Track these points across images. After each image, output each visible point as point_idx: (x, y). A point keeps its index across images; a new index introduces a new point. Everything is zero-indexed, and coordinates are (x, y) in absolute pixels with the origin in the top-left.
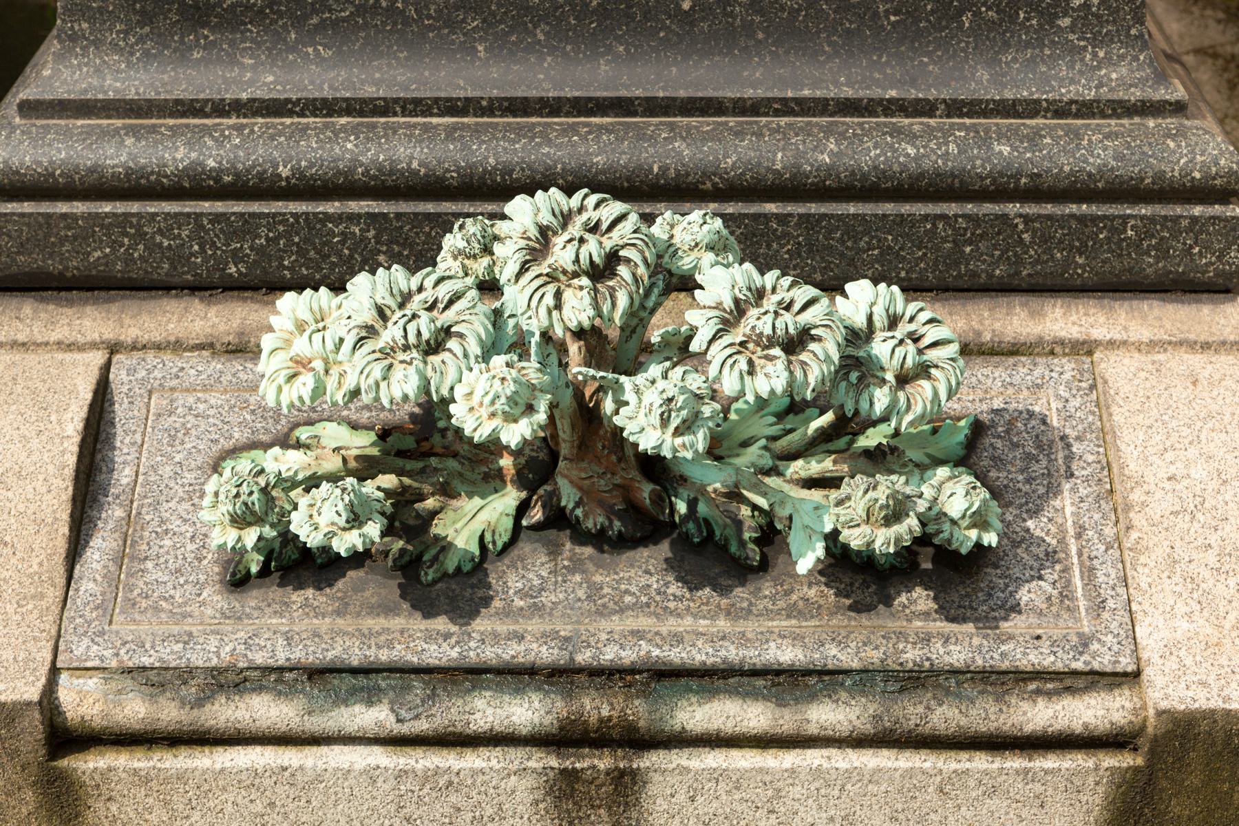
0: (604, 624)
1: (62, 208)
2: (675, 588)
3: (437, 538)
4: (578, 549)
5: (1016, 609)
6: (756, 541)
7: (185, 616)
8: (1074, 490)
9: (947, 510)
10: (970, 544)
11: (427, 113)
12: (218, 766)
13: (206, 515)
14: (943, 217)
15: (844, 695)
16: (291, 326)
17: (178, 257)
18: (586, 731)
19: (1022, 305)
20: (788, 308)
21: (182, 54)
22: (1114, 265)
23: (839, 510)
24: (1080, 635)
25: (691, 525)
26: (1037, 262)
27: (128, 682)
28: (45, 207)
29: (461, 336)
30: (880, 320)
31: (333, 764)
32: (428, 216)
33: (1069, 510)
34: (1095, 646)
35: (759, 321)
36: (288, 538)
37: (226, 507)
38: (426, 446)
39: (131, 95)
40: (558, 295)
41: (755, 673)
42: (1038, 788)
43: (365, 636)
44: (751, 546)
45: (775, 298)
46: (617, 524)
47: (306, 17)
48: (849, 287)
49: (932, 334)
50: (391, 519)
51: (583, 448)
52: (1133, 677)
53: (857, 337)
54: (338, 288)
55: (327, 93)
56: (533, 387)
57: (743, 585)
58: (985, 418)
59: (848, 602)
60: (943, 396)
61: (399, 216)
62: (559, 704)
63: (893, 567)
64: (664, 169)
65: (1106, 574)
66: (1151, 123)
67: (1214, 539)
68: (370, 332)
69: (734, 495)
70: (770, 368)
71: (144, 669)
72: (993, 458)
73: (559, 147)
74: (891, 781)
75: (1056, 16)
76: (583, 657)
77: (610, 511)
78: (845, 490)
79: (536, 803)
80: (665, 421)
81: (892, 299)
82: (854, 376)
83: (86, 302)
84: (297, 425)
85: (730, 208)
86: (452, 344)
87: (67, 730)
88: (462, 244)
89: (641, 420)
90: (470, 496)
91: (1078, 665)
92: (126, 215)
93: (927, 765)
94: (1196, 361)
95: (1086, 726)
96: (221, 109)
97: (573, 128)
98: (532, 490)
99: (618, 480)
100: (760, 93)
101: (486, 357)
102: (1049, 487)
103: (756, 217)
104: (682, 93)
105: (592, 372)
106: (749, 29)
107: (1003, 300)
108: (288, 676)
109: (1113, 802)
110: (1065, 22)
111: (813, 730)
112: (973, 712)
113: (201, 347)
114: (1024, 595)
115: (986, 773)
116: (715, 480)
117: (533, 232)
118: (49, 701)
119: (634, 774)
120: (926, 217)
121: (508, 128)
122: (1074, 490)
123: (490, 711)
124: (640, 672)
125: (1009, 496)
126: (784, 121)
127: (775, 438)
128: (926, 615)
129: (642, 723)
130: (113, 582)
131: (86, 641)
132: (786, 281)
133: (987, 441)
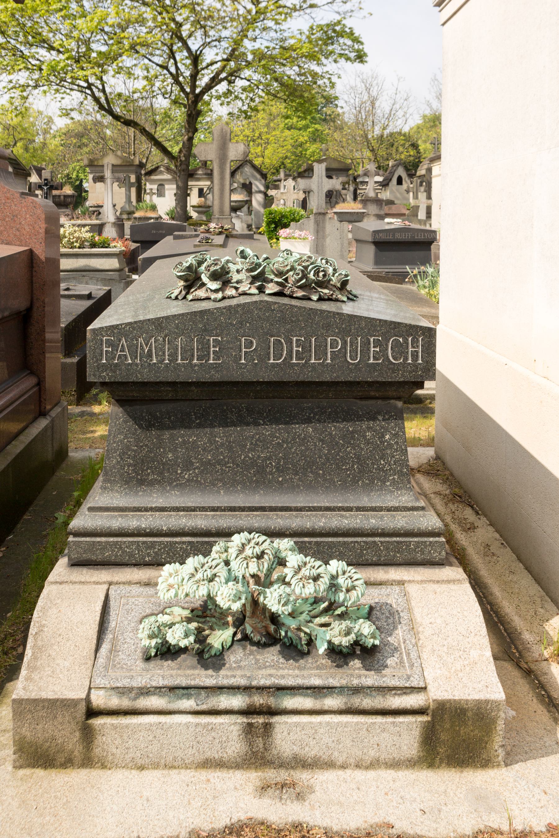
0: (261, 672)
1: (98, 539)
2: (282, 660)
3: (209, 644)
4: (252, 648)
5: (386, 666)
6: (306, 644)
7: (131, 670)
8: (402, 628)
9: (363, 632)
10: (371, 644)
11: (206, 511)
12: (139, 722)
13: (140, 636)
14: (357, 542)
15: (335, 695)
16: (168, 575)
17: (131, 555)
18: (256, 709)
19: (383, 569)
20: (314, 568)
21: (136, 493)
22: (408, 556)
23: (331, 632)
24: (407, 675)
25: (286, 639)
26: (385, 556)
27: (113, 692)
28: (93, 539)
29: (219, 576)
30: (340, 572)
31: (176, 721)
32: (206, 542)
33: (401, 634)
34: (412, 679)
35: (305, 572)
36: (165, 642)
37: (147, 632)
38: (205, 614)
39: (121, 505)
40: (247, 564)
41: (308, 688)
42: (398, 729)
43: (187, 676)
44: (305, 646)
45: (310, 565)
46: (264, 639)
47: (172, 483)
48: (331, 562)
49: (356, 576)
50: (197, 636)
51: (254, 613)
52: (424, 689)
53: (334, 578)
54: (182, 563)
55: (177, 505)
56: (240, 592)
57: (302, 659)
58: (373, 605)
59: (335, 664)
60: (360, 596)
61: (197, 542)
62: (247, 699)
63: (348, 653)
64: (275, 528)
65: (414, 655)
66: (415, 513)
67: (445, 643)
68: (193, 575)
69: (299, 629)
70: (309, 586)
71: (118, 688)
72: (376, 618)
73: (245, 521)
74: (351, 726)
75: (385, 482)
76: (254, 683)
77: (262, 635)
78: (332, 626)
79: (239, 735)
80: (279, 602)
81: (343, 566)
82: (333, 589)
83: (102, 569)
84: (166, 608)
85: (295, 539)
86: (217, 579)
87: (92, 709)
88: (219, 549)
89: (272, 602)
90: (219, 630)
91: (407, 685)
92: (117, 542)
93: (363, 720)
94: (436, 586)
95: (411, 706)
96: (146, 510)
97: (248, 515)
98: (238, 628)
99: (264, 624)
100: (302, 505)
101: (227, 583)
102: (394, 627)
103: (302, 542)
104: (280, 505)
105: (257, 587)
106: (298, 486)
107: (376, 568)
108: (163, 690)
109: (422, 734)
110: (388, 484)
111: (326, 708)
112: (376, 701)
113: (137, 583)
114: (389, 662)
115: (381, 723)
116: (293, 624)
117: (240, 545)
118: (88, 699)
119: (270, 724)
120: (352, 542)
121: (230, 515)
122: (402, 628)
123: (225, 702)
124: (272, 688)
125: (382, 630)
126: (309, 513)
127: (310, 611)
128: (359, 668)
129: (273, 706)
130: (109, 658)
131: (100, 678)
132: (313, 560)
133: (374, 612)
